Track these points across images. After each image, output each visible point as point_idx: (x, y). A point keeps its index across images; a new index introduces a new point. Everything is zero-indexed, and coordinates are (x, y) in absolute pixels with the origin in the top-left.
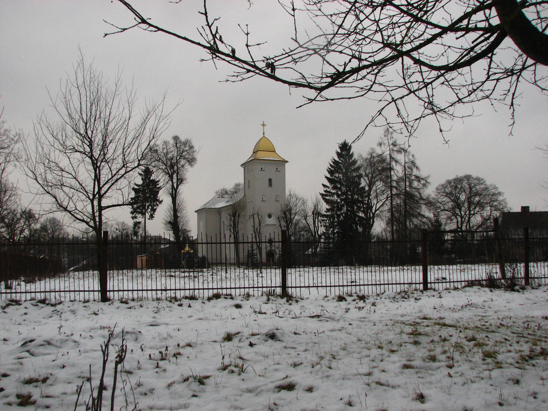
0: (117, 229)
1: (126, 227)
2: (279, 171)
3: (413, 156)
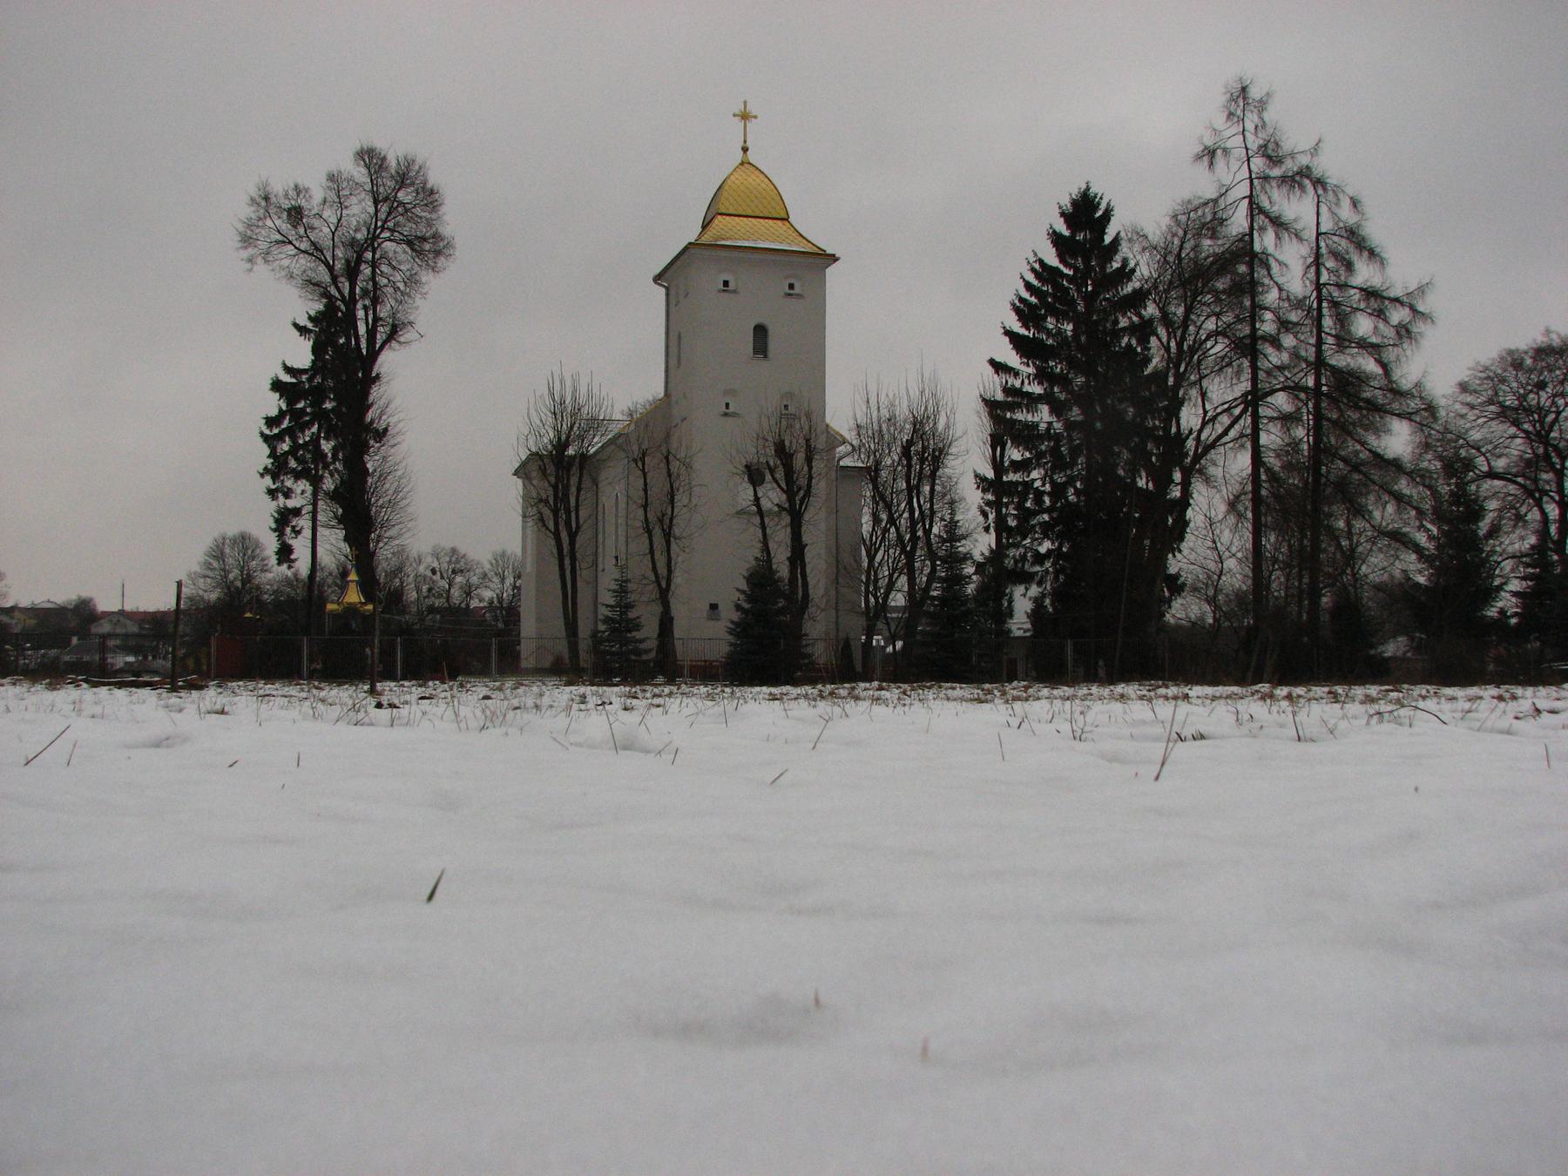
0: (434, 571)
1: (462, 565)
2: (799, 296)
3: (1355, 203)
